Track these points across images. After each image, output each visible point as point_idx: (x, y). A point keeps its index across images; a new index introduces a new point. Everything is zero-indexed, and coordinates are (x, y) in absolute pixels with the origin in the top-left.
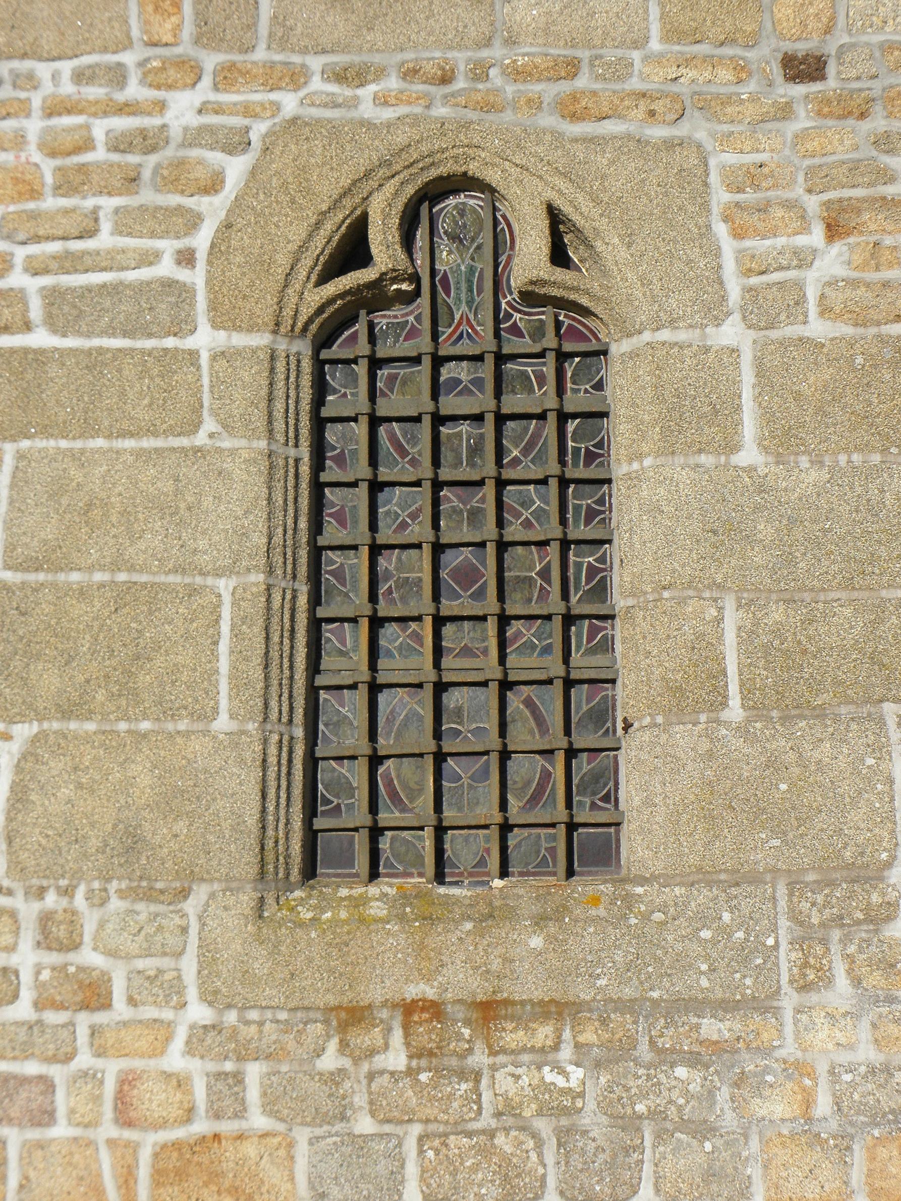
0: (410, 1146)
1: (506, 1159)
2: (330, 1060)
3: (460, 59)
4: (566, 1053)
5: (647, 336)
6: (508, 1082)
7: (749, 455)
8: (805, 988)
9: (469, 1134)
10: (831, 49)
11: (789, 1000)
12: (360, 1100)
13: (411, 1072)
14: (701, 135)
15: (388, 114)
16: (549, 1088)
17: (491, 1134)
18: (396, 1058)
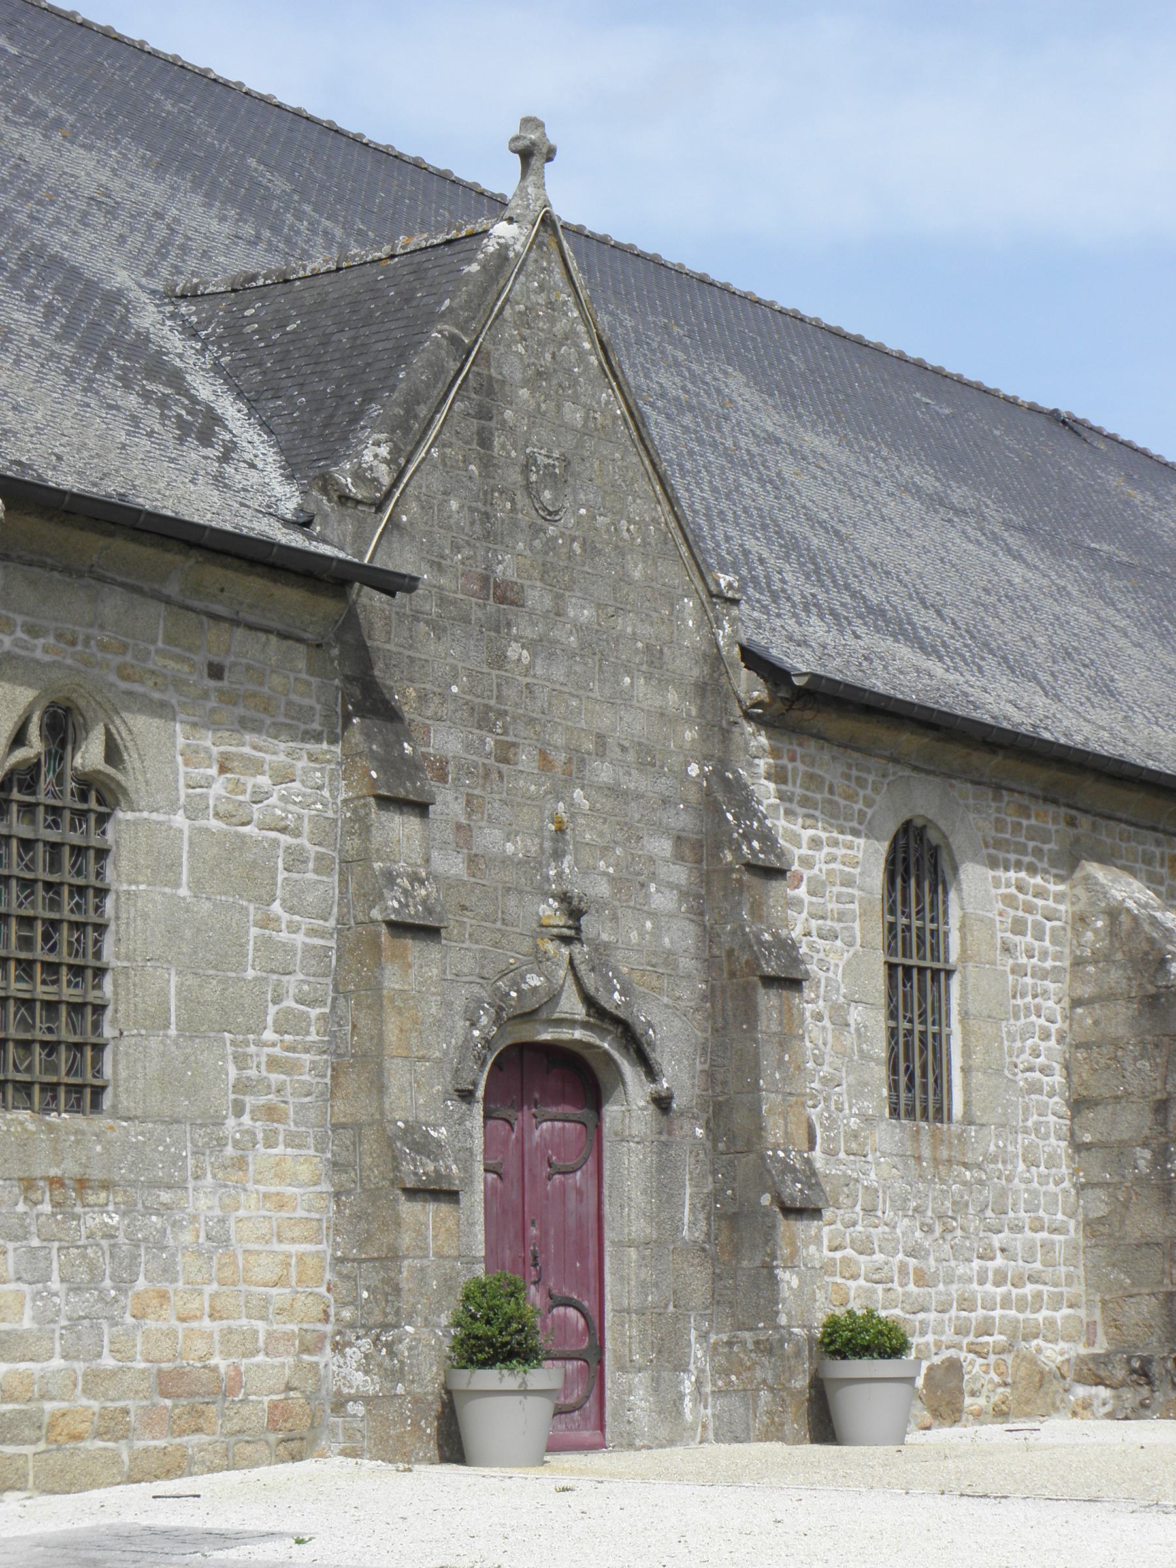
0: (54, 1252)
1: (91, 1259)
2: (21, 1208)
3: (81, 632)
4: (111, 1208)
5: (145, 814)
6: (93, 1220)
7: (183, 892)
8: (197, 1178)
9: (78, 1247)
10: (227, 663)
11: (191, 1184)
12: (33, 1229)
13: (54, 1214)
14: (174, 701)
15: (47, 658)
16: (106, 1225)
17: (85, 1247)
18: (47, 1208)
